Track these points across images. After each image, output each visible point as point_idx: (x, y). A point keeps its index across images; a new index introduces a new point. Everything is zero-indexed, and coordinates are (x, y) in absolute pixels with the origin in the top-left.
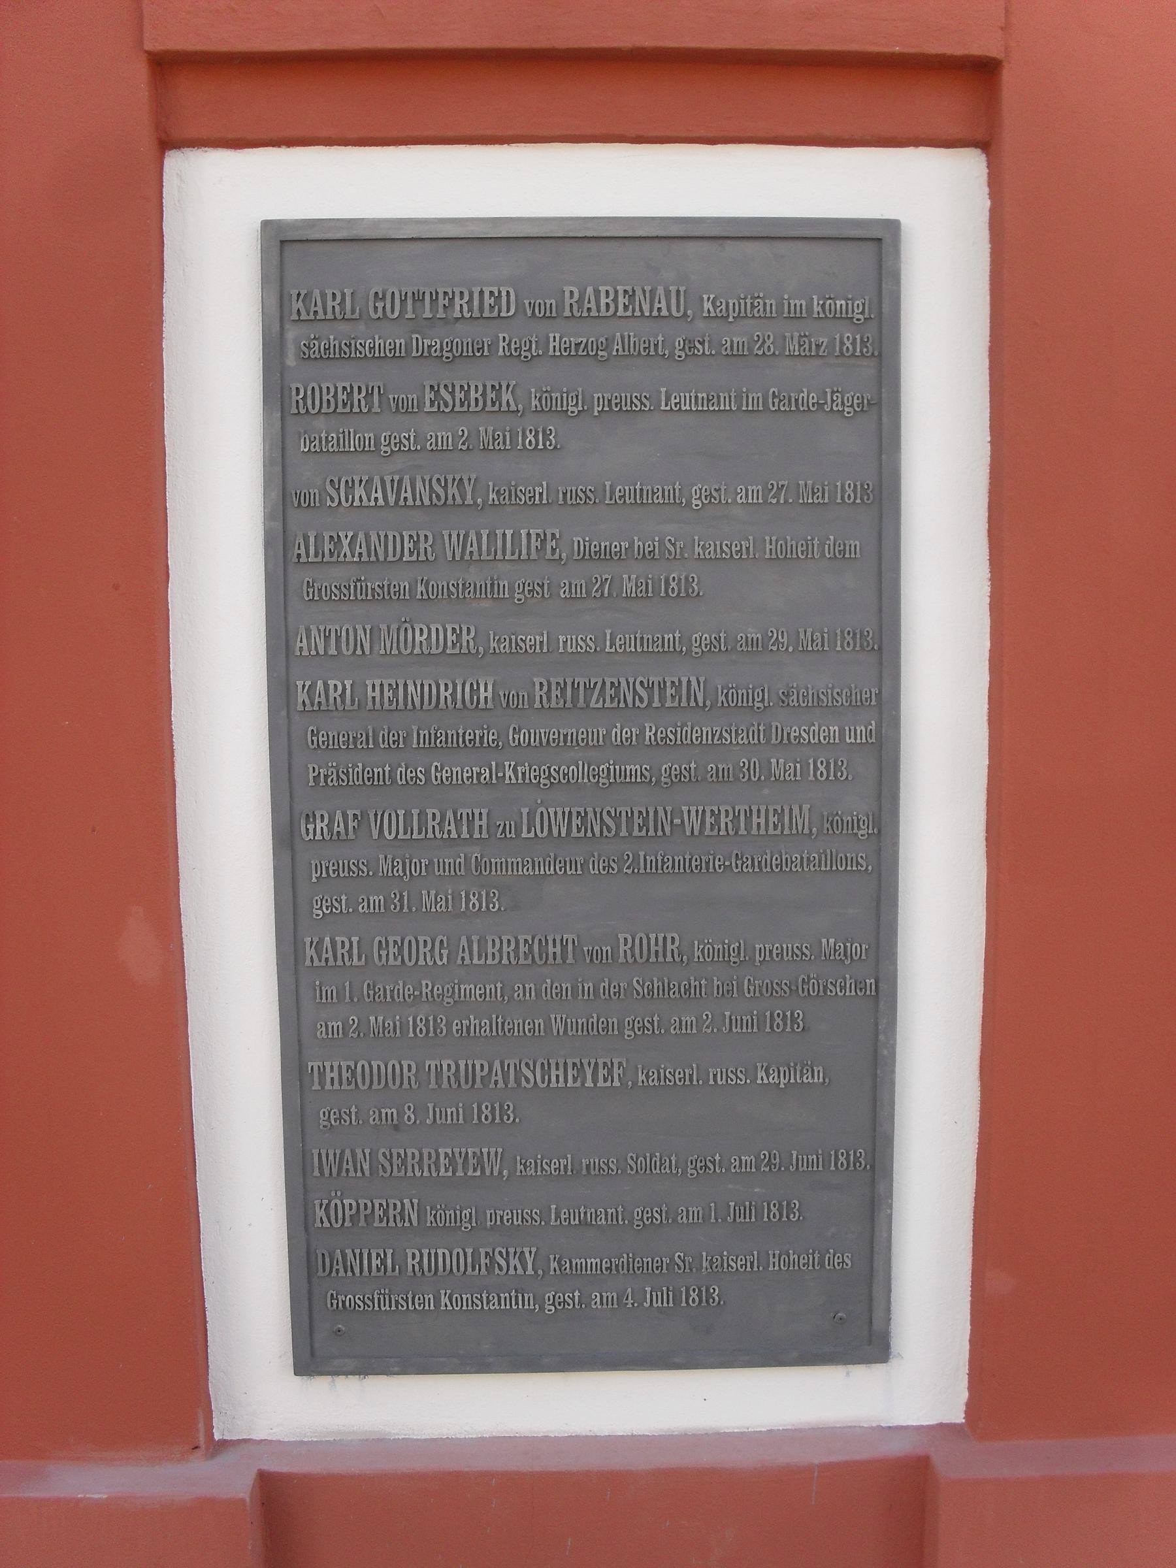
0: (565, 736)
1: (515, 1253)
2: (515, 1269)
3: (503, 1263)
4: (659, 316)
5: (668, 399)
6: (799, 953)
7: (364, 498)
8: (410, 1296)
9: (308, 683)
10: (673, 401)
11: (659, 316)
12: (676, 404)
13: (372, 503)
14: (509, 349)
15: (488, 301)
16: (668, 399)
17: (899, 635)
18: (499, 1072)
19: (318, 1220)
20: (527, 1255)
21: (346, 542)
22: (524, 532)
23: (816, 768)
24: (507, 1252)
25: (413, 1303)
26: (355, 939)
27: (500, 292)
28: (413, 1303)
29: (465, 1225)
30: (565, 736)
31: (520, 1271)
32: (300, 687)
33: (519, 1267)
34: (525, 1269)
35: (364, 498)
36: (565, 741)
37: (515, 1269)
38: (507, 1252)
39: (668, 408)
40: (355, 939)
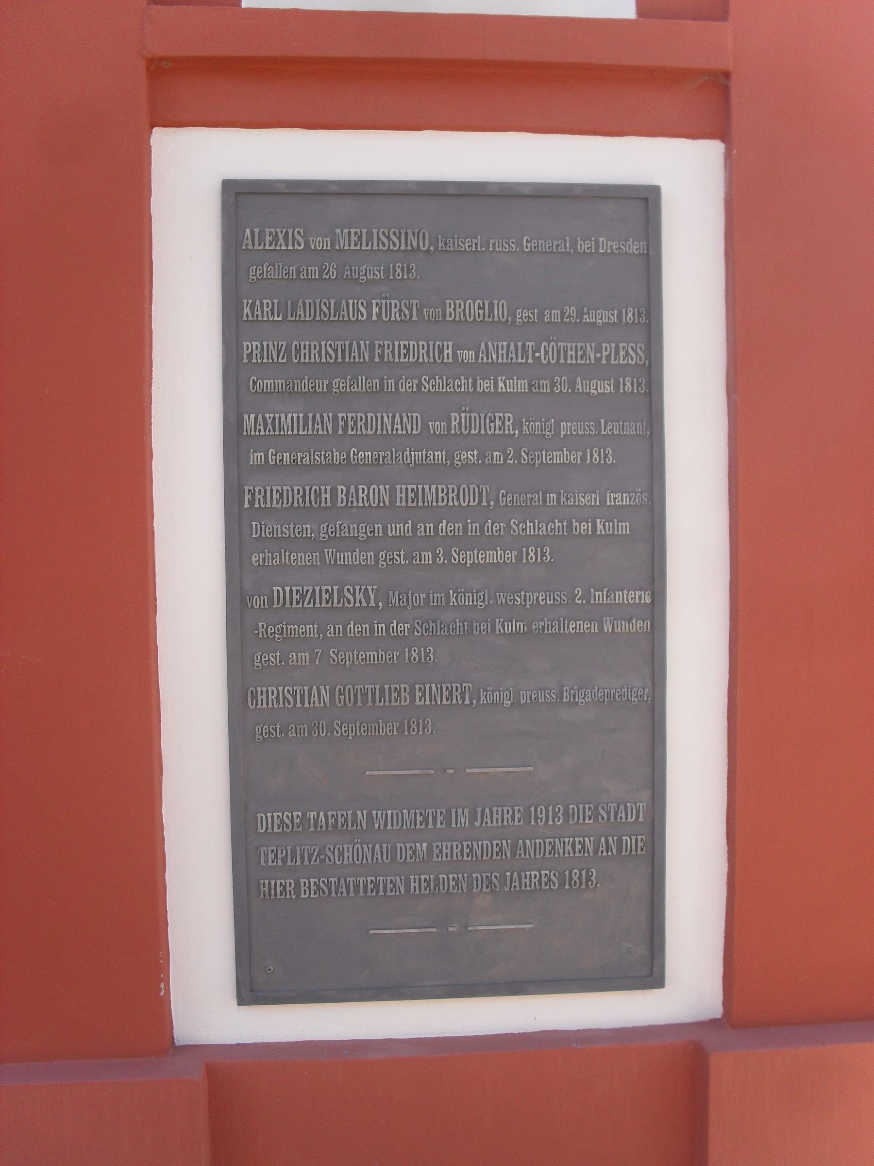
0: (364, 694)
2: (361, 602)
3: (350, 597)
6: (559, 599)
8: (292, 526)
9: (250, 301)
15: (325, 596)
17: (467, 1038)
19: (245, 315)
20: (370, 592)
21: (281, 236)
23: (592, 456)
25: (294, 532)
26: (276, 301)
27: (332, 589)
28: (294, 532)
29: (362, 278)
30: (364, 694)
31: (364, 604)
32: (245, 304)
33: (363, 600)
34: (368, 602)
36: (364, 702)
37: (361, 602)
38: (354, 590)
40: (276, 301)
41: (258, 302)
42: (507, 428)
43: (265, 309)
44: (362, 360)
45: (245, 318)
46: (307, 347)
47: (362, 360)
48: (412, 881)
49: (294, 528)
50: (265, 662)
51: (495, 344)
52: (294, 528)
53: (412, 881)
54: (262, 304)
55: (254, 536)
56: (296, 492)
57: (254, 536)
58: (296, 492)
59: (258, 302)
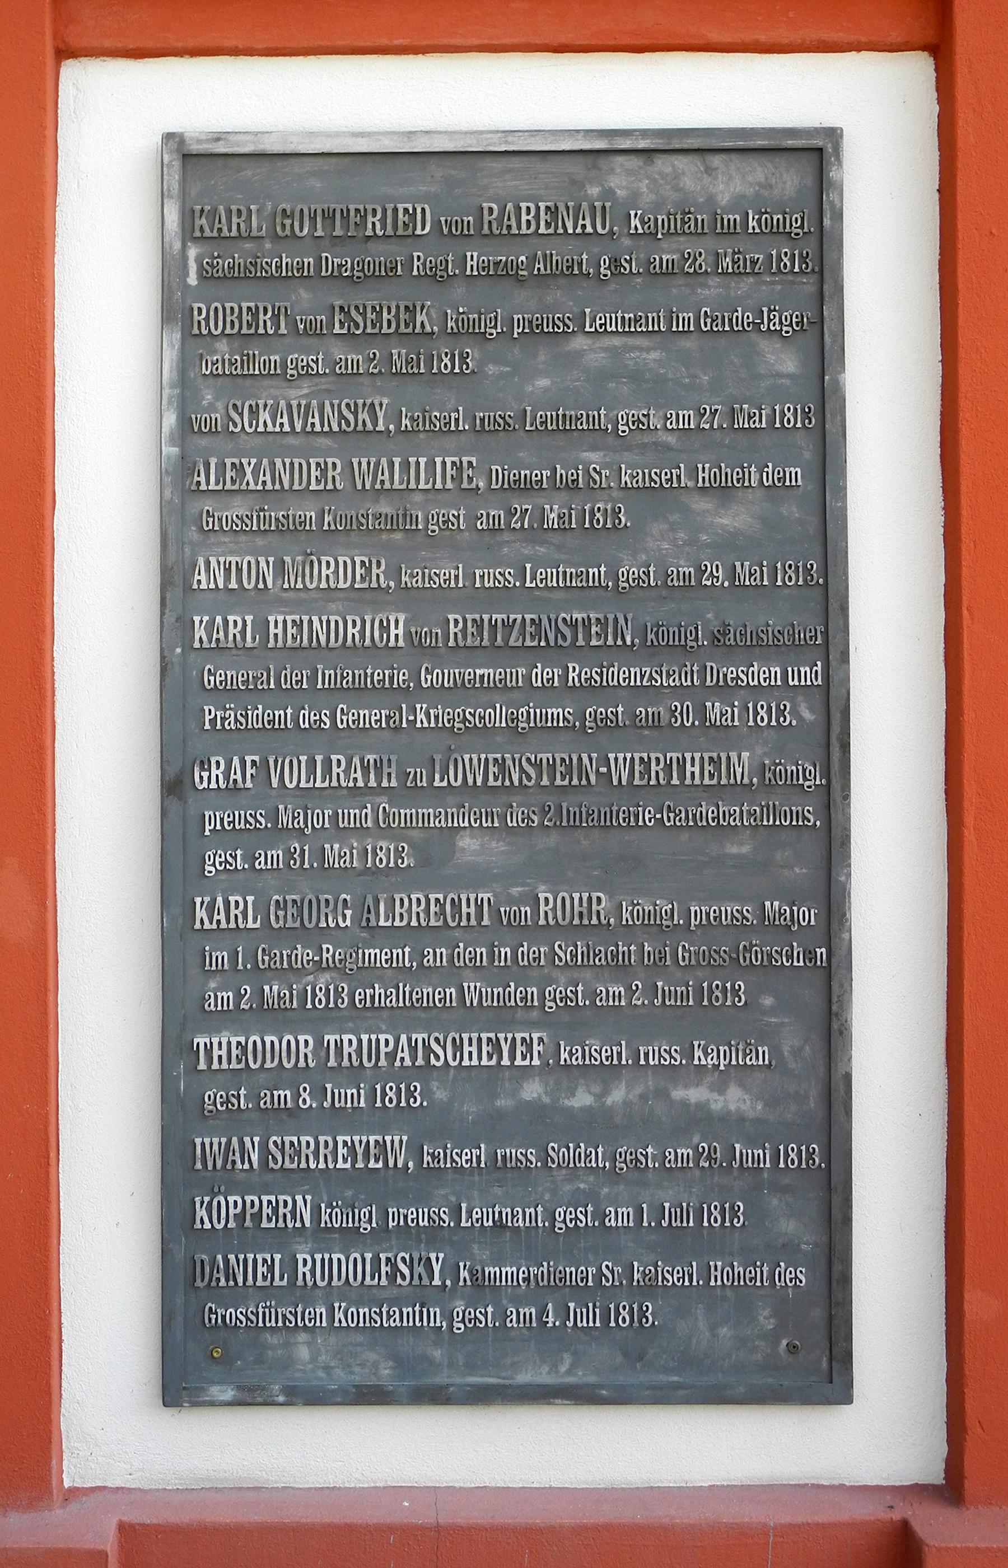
8: (299, 1310)
13: (278, 429)
25: (303, 1319)
28: (303, 1319)
41: (220, 900)
42: (374, 578)
43: (233, 911)
44: (277, 487)
45: (197, 645)
46: (280, 625)
47: (277, 487)
48: (469, 258)
49: (303, 1313)
50: (602, 720)
51: (288, 461)
52: (303, 1313)
53: (469, 258)
54: (227, 903)
55: (323, 274)
56: (228, 311)
57: (323, 274)
58: (228, 311)
59: (220, 900)
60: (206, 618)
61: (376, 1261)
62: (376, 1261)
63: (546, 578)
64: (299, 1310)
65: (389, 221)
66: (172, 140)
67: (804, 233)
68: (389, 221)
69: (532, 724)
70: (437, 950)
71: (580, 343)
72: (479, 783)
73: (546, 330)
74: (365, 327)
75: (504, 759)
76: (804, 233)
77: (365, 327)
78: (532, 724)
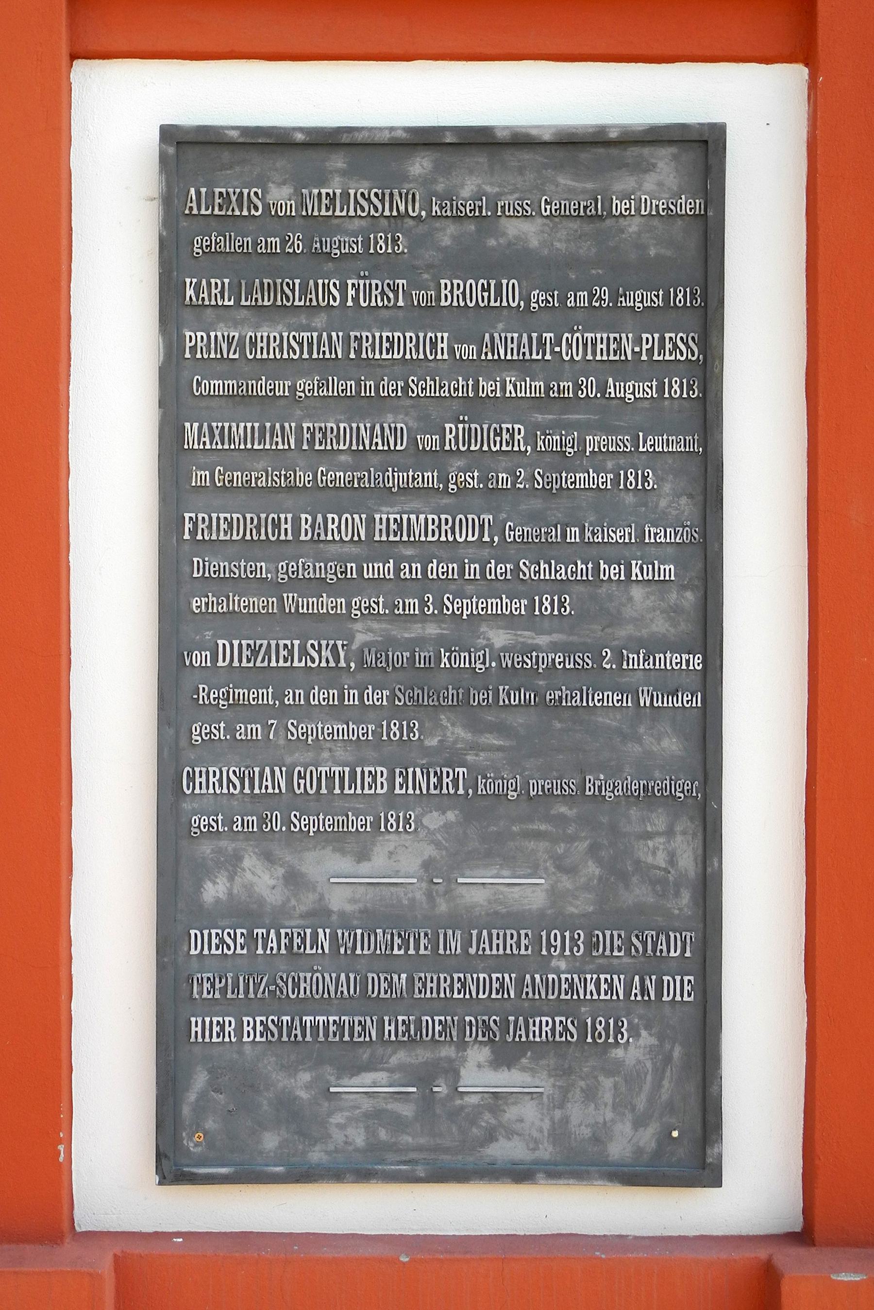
1: (327, 645)
2: (327, 661)
4: (190, 214)
5: (645, 442)
7: (194, 299)
8: (243, 564)
10: (649, 443)
11: (190, 214)
12: (651, 446)
13: (200, 302)
14: (209, 698)
16: (645, 442)
18: (298, 1028)
22: (359, 770)
24: (320, 645)
25: (245, 571)
28: (245, 571)
33: (331, 659)
34: (337, 661)
35: (194, 299)
37: (327, 661)
38: (320, 645)
39: (645, 450)
59: (204, 282)
60: (194, 280)
61: (662, 339)
62: (662, 339)
63: (333, 824)
64: (243, 564)
65: (213, 346)
66: (168, 133)
67: (229, 704)
68: (213, 346)
69: (231, 702)
70: (406, 600)
71: (619, 1053)
72: (648, 704)
73: (611, 450)
74: (235, 948)
75: (573, 979)
76: (229, 704)
77: (235, 948)
78: (231, 702)
